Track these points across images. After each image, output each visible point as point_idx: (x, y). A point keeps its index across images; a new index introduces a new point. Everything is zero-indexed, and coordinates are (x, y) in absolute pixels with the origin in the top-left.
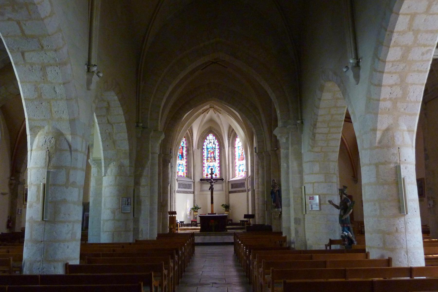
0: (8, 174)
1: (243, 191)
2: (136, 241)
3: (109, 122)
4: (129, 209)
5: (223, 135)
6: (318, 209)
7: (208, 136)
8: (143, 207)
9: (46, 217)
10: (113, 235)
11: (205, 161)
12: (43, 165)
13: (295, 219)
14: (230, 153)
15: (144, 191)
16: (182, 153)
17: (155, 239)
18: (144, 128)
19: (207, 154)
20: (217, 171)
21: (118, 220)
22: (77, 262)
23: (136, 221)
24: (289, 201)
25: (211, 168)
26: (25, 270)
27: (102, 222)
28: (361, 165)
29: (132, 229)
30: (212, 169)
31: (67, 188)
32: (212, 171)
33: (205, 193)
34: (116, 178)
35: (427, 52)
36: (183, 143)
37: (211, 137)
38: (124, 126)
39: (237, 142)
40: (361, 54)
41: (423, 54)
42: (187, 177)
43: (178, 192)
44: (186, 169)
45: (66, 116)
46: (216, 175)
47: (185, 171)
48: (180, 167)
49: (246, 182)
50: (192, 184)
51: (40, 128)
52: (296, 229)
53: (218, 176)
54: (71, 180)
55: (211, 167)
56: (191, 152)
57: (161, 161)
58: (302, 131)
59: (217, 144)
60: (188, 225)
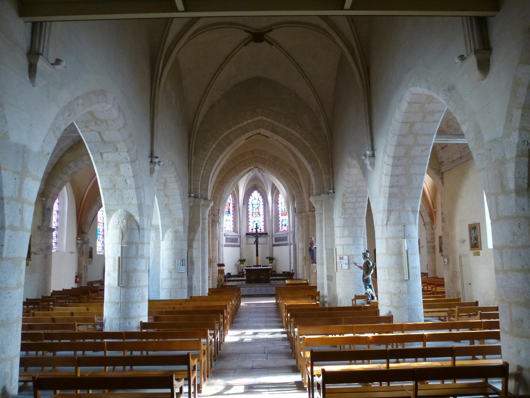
0: (75, 234)
1: (285, 245)
2: (191, 297)
3: (166, 195)
4: (184, 269)
5: (266, 190)
6: (347, 268)
7: (253, 192)
8: (195, 267)
9: (121, 284)
10: (171, 292)
11: (250, 217)
12: (118, 242)
13: (328, 276)
14: (274, 209)
15: (196, 254)
16: (229, 209)
17: (207, 295)
18: (195, 197)
19: (253, 210)
20: (261, 226)
21: (175, 279)
22: (145, 320)
23: (190, 279)
24: (323, 260)
25: (256, 223)
26: (106, 325)
27: (161, 280)
28: (376, 238)
29: (186, 286)
30: (257, 224)
31: (137, 259)
32: (257, 226)
33: (251, 246)
34: (172, 242)
35: (426, 149)
36: (230, 200)
37: (256, 194)
38: (179, 198)
39: (280, 199)
40: (375, 147)
41: (422, 151)
42: (234, 231)
43: (226, 246)
44: (233, 224)
45: (135, 202)
46: (260, 229)
47: (232, 226)
48: (227, 223)
49: (288, 236)
50: (239, 238)
51: (114, 211)
52: (328, 285)
53: (263, 231)
54: (140, 253)
55: (256, 221)
56: (238, 208)
57: (210, 222)
58: (333, 198)
59: (262, 200)
60: (235, 276)
